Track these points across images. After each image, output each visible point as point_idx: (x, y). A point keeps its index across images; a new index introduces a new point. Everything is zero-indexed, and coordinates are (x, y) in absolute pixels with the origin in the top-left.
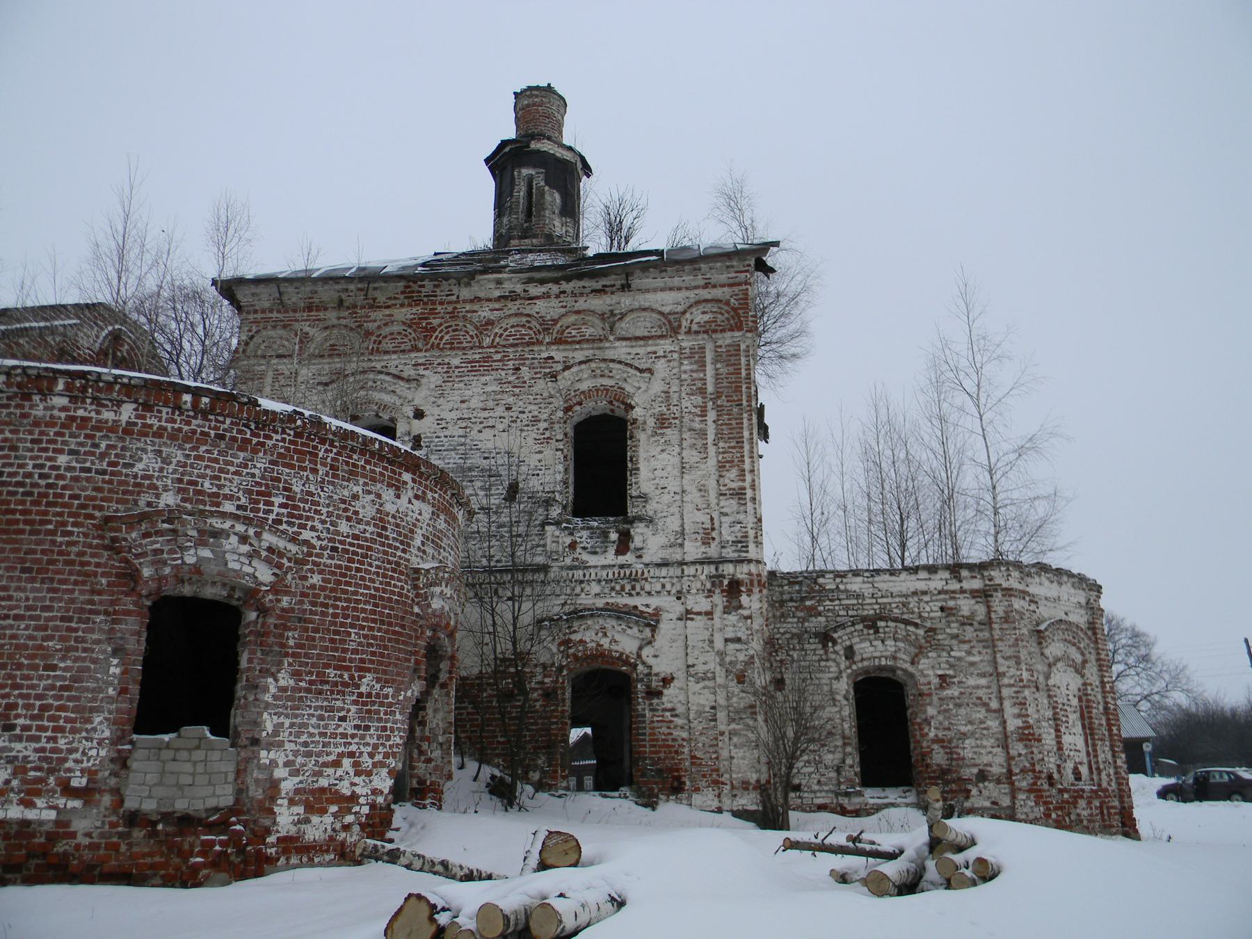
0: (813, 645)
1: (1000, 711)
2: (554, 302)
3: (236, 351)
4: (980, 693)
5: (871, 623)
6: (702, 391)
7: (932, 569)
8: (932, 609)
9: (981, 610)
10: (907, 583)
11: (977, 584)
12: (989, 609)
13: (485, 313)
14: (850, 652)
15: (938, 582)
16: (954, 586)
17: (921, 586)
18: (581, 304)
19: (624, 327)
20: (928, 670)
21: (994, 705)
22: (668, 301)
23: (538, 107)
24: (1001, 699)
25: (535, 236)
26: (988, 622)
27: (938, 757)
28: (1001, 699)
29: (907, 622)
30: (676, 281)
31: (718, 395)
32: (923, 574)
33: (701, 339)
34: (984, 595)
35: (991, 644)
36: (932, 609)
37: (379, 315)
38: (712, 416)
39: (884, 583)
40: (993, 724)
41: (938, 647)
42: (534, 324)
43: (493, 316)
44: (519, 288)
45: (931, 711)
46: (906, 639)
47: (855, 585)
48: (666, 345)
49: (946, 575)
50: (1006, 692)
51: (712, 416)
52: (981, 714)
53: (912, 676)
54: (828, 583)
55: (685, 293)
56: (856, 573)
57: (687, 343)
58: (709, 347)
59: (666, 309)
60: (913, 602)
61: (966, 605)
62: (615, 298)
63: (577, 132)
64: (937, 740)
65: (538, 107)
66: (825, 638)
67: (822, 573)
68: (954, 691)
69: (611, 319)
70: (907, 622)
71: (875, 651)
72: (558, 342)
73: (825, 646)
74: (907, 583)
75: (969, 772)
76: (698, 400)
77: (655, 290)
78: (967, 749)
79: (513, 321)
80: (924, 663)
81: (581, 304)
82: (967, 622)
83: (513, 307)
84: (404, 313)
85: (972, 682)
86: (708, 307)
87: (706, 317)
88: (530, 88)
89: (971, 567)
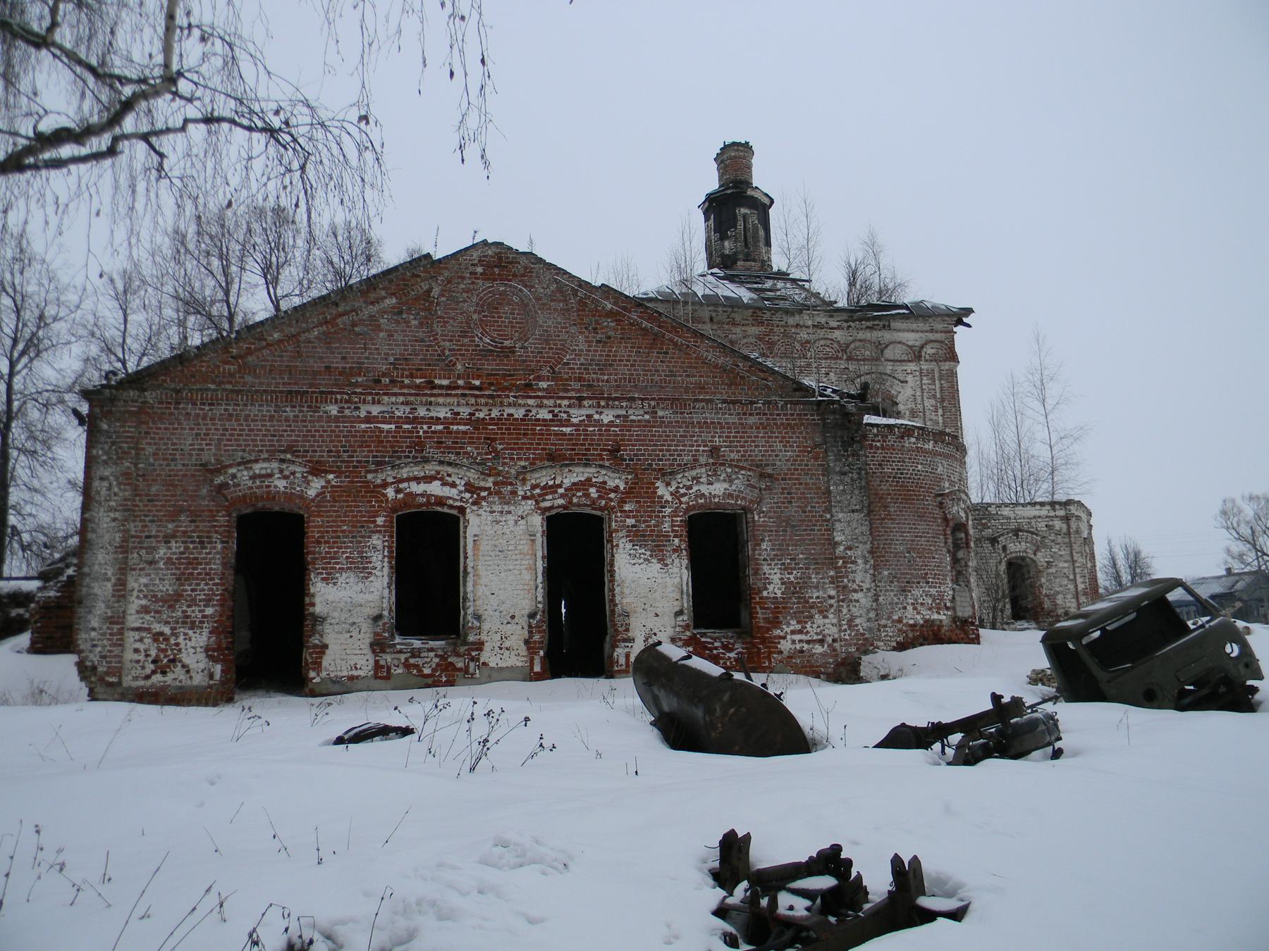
0: (987, 545)
1: (1075, 580)
2: (845, 332)
3: (351, 286)
4: (1065, 571)
5: (1016, 532)
6: (934, 396)
7: (1042, 504)
8: (1041, 526)
9: (1064, 527)
10: (1031, 512)
11: (1062, 513)
12: (1069, 527)
13: (804, 335)
14: (1004, 548)
15: (1044, 512)
16: (1052, 514)
17: (1037, 513)
18: (861, 335)
19: (888, 353)
20: (1041, 558)
21: (1071, 577)
22: (912, 338)
23: (735, 159)
24: (1075, 574)
25: (754, 260)
26: (1069, 533)
27: (1047, 604)
28: (1075, 574)
29: (1032, 533)
30: (914, 326)
31: (943, 400)
32: (1038, 507)
33: (933, 365)
34: (1066, 519)
35: (1070, 545)
36: (1041, 526)
37: (738, 330)
38: (940, 411)
39: (1020, 511)
40: (1071, 587)
41: (1045, 547)
42: (835, 345)
43: (812, 337)
44: (823, 321)
45: (1043, 580)
46: (1030, 542)
47: (1006, 512)
48: (912, 367)
49: (1048, 507)
50: (1077, 570)
51: (940, 411)
52: (1065, 582)
53: (1034, 561)
54: (992, 510)
55: (920, 335)
56: (1007, 505)
57: (925, 366)
58: (936, 369)
59: (910, 343)
60: (1033, 521)
61: (1058, 524)
62: (880, 334)
63: (762, 178)
64: (1047, 596)
65: (735, 159)
66: (994, 541)
67: (989, 505)
68: (1052, 570)
69: (881, 347)
70: (1032, 533)
71: (1017, 548)
72: (850, 359)
73: (993, 545)
74: (1031, 512)
75: (1060, 611)
76: (933, 402)
77: (904, 331)
78: (1059, 601)
79: (822, 342)
80: (1039, 554)
81: (861, 335)
82: (1058, 533)
83: (821, 333)
84: (754, 330)
85: (1061, 565)
86: (935, 345)
87: (933, 351)
88: (734, 144)
89: (1060, 503)
